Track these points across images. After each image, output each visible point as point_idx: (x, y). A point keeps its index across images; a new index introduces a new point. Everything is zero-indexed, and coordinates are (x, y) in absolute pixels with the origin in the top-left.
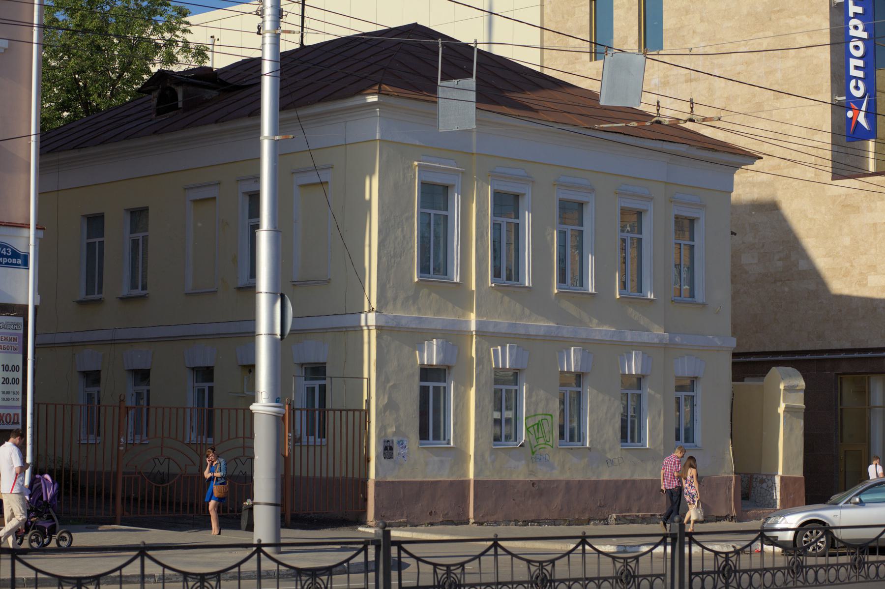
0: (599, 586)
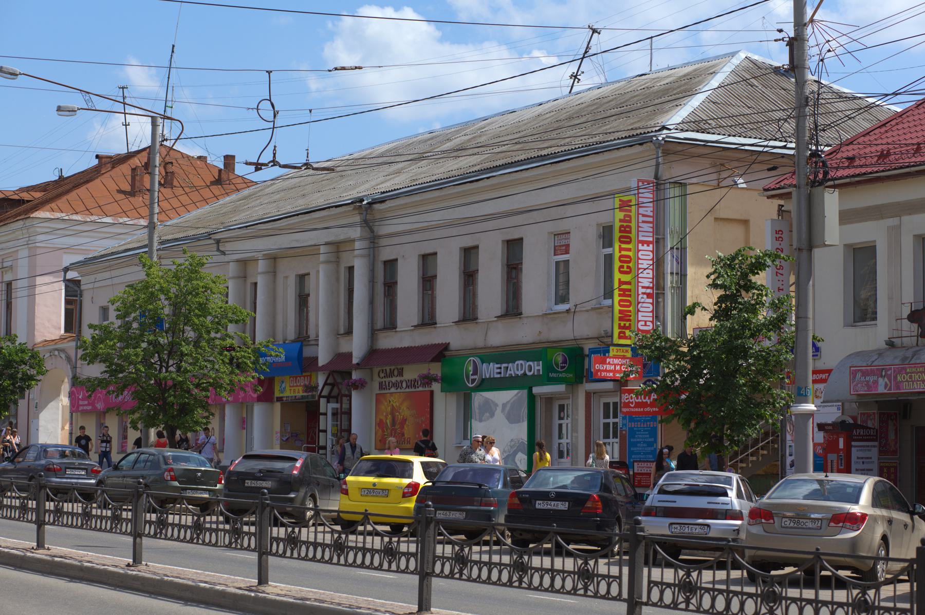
0: (801, 610)
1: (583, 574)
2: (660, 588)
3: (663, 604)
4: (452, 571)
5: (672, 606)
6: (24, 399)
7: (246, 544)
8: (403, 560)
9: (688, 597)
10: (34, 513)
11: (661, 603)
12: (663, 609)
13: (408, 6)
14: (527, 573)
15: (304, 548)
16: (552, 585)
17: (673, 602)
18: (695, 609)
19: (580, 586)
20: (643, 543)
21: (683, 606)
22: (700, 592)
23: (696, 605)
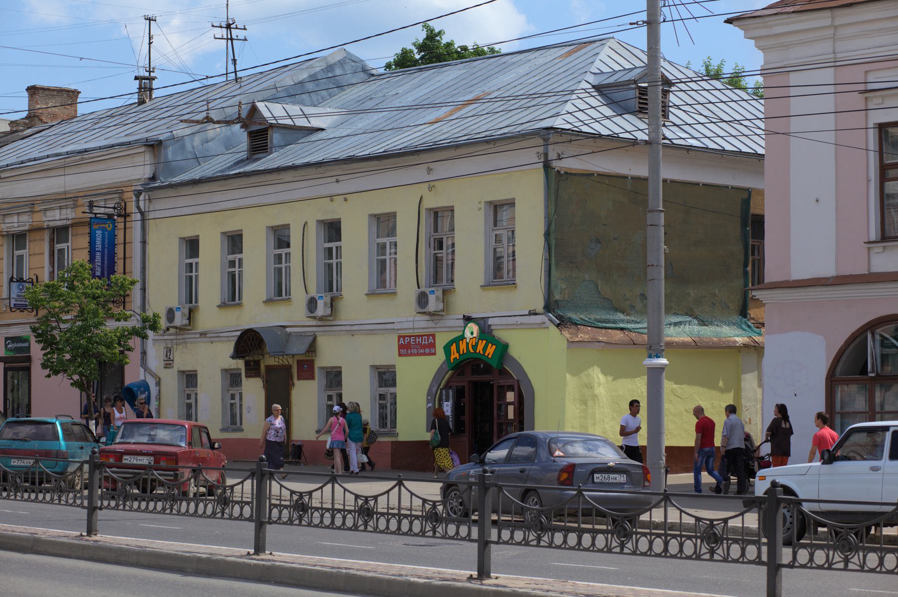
1: (431, 517)
2: (679, 541)
5: (420, 534)
8: (316, 514)
9: (434, 526)
11: (565, 546)
12: (514, 546)
18: (372, 530)
19: (218, 510)
21: (297, 522)
22: (727, 543)
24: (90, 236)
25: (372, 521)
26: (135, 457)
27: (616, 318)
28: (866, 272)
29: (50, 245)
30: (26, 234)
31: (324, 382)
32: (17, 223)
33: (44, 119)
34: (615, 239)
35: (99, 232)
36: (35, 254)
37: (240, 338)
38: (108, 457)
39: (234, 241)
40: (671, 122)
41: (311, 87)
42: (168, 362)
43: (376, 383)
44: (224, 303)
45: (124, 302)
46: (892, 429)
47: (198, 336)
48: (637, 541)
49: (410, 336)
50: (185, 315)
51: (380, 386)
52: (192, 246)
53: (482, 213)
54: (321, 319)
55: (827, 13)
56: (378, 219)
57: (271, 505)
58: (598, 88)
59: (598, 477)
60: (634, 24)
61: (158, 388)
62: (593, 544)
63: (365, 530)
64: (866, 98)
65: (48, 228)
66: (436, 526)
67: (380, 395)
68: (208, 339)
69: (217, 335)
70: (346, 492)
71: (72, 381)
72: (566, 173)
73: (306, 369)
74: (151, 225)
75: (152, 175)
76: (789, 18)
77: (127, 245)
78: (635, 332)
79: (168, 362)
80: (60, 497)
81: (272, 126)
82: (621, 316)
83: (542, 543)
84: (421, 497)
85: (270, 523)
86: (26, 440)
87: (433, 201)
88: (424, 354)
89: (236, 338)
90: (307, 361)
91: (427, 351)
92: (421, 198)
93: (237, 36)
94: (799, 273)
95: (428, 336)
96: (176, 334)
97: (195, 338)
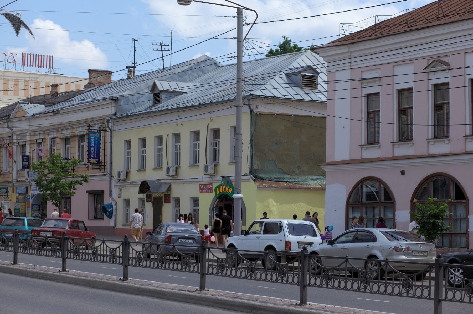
2: (421, 289)
3: (272, 281)
4: (136, 264)
6: (367, 201)
7: (144, 265)
10: (60, 252)
13: (90, 40)
14: (225, 269)
15: (118, 259)
16: (266, 278)
17: (399, 292)
20: (443, 268)
22: (333, 279)
23: (331, 285)
24: (89, 140)
25: (224, 271)
26: (45, 232)
27: (284, 177)
28: (360, 158)
29: (78, 143)
30: (69, 138)
31: (174, 203)
32: (66, 133)
33: (95, 85)
34: (285, 142)
35: (93, 138)
36: (73, 147)
37: (141, 185)
38: (35, 232)
39: (143, 142)
40: (319, 90)
41: (189, 73)
42: (120, 195)
43: (193, 205)
44: (140, 169)
45: (104, 169)
46: (265, 222)
47: (130, 184)
48: (372, 286)
49: (204, 184)
50: (125, 175)
51: (194, 206)
52: (129, 143)
53: (229, 132)
54: (172, 176)
55: (346, 46)
56: (194, 133)
57: (209, 265)
58: (287, 75)
59: (181, 241)
60: (230, 57)
61: (115, 206)
62: (454, 297)
63: (407, 296)
64: (362, 83)
65: (78, 135)
66: (367, 286)
67: (194, 210)
68: (134, 185)
69: (136, 183)
70: (133, 250)
71: (53, 203)
72: (260, 114)
73: (168, 200)
74: (114, 133)
75: (115, 113)
76: (333, 48)
77: (106, 143)
78: (293, 183)
79: (120, 195)
80: (222, 271)
81: (161, 91)
82: (287, 176)
83: (410, 295)
84: (218, 257)
85: (309, 286)
86: (12, 226)
87: (214, 126)
88: (209, 192)
89: (139, 185)
90: (168, 195)
91: (210, 191)
92: (208, 124)
93: (165, 49)
94: (338, 158)
95: (210, 184)
96: (122, 183)
97: (129, 185)
